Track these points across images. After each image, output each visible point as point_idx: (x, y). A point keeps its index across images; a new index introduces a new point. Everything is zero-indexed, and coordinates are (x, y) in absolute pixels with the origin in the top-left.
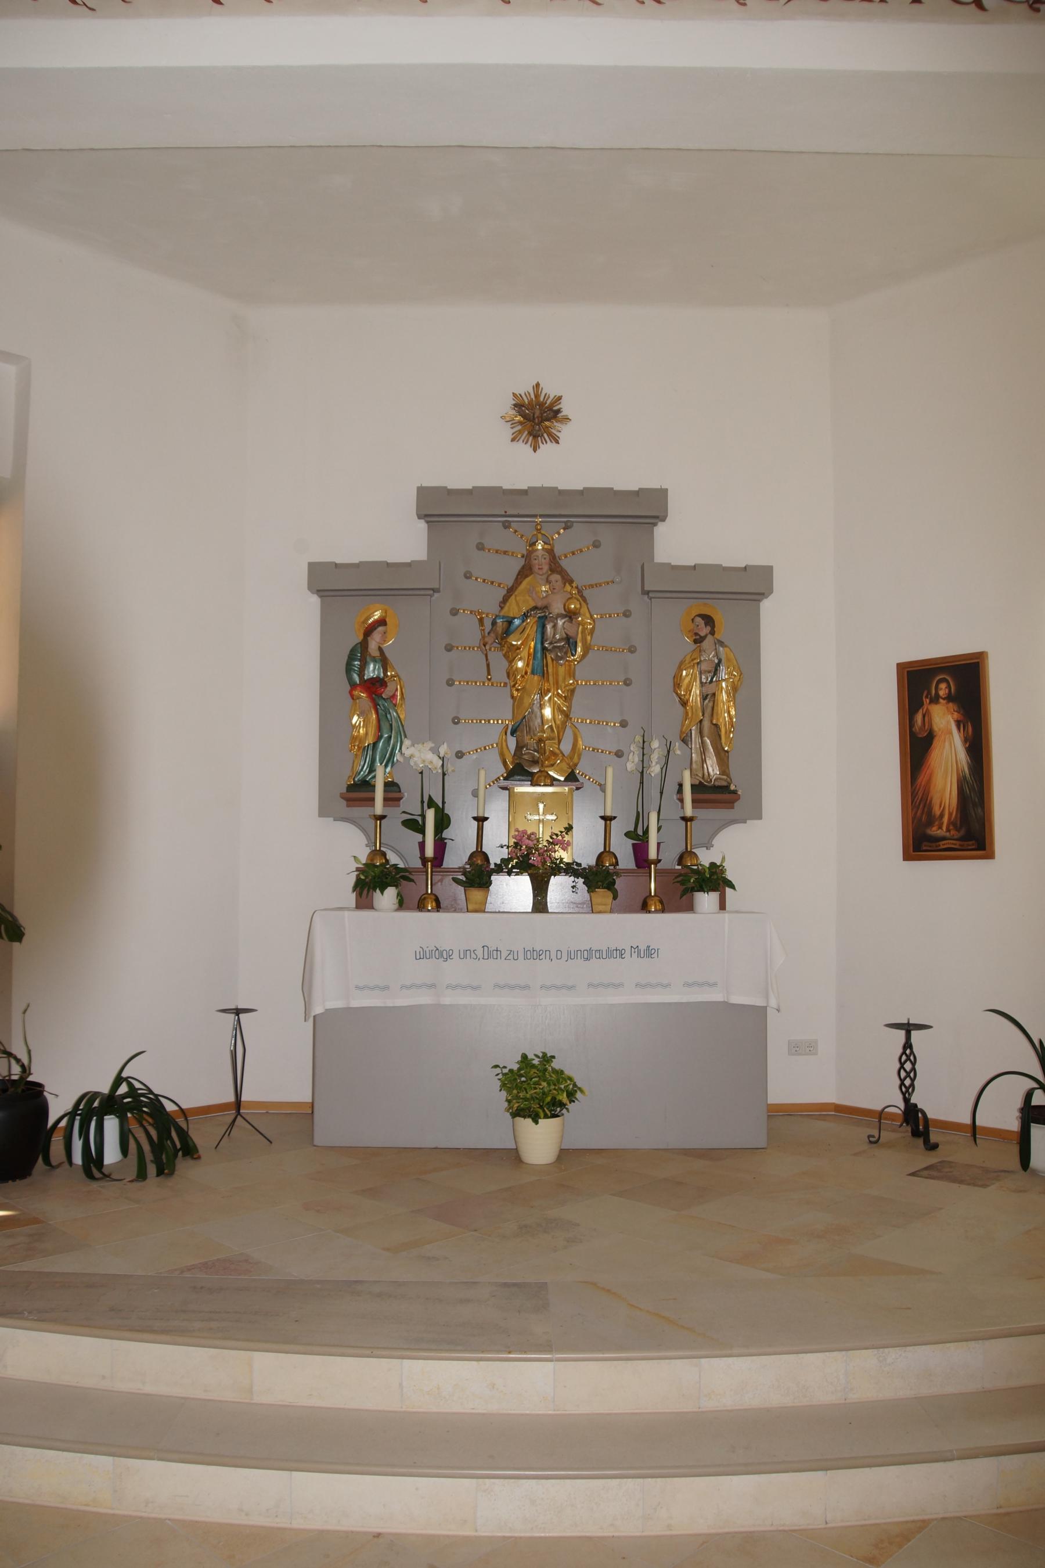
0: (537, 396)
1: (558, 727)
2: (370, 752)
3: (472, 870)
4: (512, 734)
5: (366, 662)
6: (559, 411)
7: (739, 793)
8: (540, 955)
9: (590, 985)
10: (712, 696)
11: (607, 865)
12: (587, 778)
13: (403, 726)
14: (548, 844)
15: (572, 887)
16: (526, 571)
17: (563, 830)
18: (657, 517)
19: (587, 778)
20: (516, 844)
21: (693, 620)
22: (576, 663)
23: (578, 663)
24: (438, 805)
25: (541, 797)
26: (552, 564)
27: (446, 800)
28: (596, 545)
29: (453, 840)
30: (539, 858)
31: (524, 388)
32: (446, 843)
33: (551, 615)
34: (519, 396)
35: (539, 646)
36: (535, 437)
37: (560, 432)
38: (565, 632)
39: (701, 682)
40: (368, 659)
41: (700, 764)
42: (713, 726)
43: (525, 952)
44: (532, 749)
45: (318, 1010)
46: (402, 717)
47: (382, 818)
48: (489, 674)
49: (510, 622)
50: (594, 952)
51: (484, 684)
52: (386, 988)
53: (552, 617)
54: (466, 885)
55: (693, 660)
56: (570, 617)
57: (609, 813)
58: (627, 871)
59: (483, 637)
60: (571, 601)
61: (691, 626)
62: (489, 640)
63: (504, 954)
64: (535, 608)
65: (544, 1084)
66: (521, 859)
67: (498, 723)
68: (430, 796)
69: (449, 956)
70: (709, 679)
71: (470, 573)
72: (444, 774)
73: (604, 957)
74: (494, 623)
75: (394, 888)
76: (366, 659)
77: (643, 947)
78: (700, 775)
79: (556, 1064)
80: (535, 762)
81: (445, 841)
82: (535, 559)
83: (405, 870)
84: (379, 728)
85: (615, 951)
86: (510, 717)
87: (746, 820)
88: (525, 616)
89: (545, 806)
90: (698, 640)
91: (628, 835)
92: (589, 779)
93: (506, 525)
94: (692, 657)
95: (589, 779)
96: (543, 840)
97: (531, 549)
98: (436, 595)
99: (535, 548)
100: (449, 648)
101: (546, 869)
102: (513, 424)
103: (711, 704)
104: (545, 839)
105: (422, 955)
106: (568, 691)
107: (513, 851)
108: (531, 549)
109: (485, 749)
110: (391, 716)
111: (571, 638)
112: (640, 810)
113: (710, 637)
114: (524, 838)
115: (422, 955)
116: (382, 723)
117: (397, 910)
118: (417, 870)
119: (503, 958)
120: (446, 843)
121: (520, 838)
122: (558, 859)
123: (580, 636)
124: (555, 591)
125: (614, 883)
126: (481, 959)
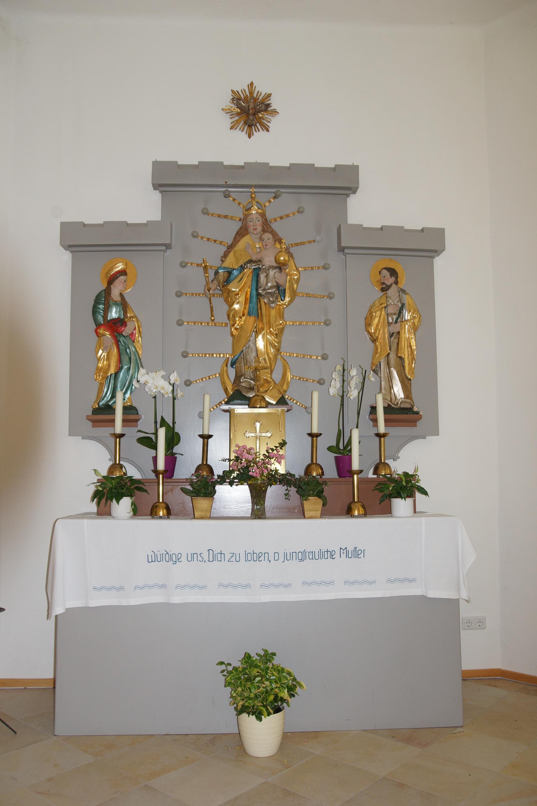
0: (251, 93)
1: (270, 359)
2: (112, 381)
3: (198, 481)
4: (232, 366)
5: (109, 306)
6: (268, 105)
7: (421, 414)
8: (259, 557)
9: (304, 583)
10: (397, 334)
11: (315, 475)
12: (295, 402)
13: (140, 359)
14: (265, 458)
15: (285, 494)
16: (242, 232)
17: (278, 445)
18: (349, 189)
19: (295, 402)
20: (237, 458)
21: (380, 272)
22: (285, 306)
23: (287, 307)
24: (169, 425)
25: (257, 417)
26: (265, 226)
27: (176, 420)
28: (300, 211)
29: (182, 455)
30: (258, 471)
31: (241, 86)
32: (176, 457)
33: (264, 267)
34: (236, 92)
35: (254, 292)
36: (250, 126)
37: (270, 122)
38: (276, 281)
39: (388, 323)
40: (111, 302)
41: (388, 389)
42: (398, 359)
43: (246, 554)
44: (249, 378)
45: (58, 610)
46: (140, 352)
47: (121, 436)
48: (212, 315)
49: (230, 273)
50: (307, 553)
51: (208, 325)
52: (121, 588)
53: (265, 268)
54: (192, 494)
55: (381, 304)
56: (280, 268)
57: (315, 431)
58: (332, 480)
59: (207, 283)
60: (280, 254)
61: (378, 277)
62: (213, 286)
63: (228, 556)
64: (250, 261)
65: (267, 683)
66: (242, 471)
67: (220, 357)
68: (162, 417)
69: (178, 559)
70: (394, 320)
71: (197, 233)
72: (174, 399)
73: (317, 558)
74: (216, 273)
75: (129, 498)
76: (109, 303)
77: (350, 549)
78: (389, 399)
79: (276, 661)
80: (251, 389)
81: (176, 456)
82: (251, 221)
83: (138, 481)
84: (120, 361)
85: (326, 553)
86: (231, 352)
87: (426, 436)
88: (242, 268)
89: (261, 425)
90: (385, 289)
91: (330, 449)
92: (296, 403)
93: (227, 195)
94: (381, 302)
95: (296, 403)
96: (260, 455)
97: (246, 213)
98: (169, 251)
99: (250, 212)
100: (179, 295)
101: (263, 480)
102: (232, 116)
103: (396, 341)
104: (262, 453)
105: (154, 559)
106: (279, 329)
107: (234, 464)
108: (246, 213)
109: (209, 378)
110: (130, 351)
111: (280, 286)
112: (341, 428)
113: (394, 285)
114: (244, 452)
115: (154, 559)
116: (122, 357)
117: (131, 518)
118: (150, 481)
119: (227, 560)
120: (176, 457)
121: (240, 453)
122: (273, 471)
123: (288, 284)
124: (267, 247)
125: (322, 491)
126: (207, 561)
